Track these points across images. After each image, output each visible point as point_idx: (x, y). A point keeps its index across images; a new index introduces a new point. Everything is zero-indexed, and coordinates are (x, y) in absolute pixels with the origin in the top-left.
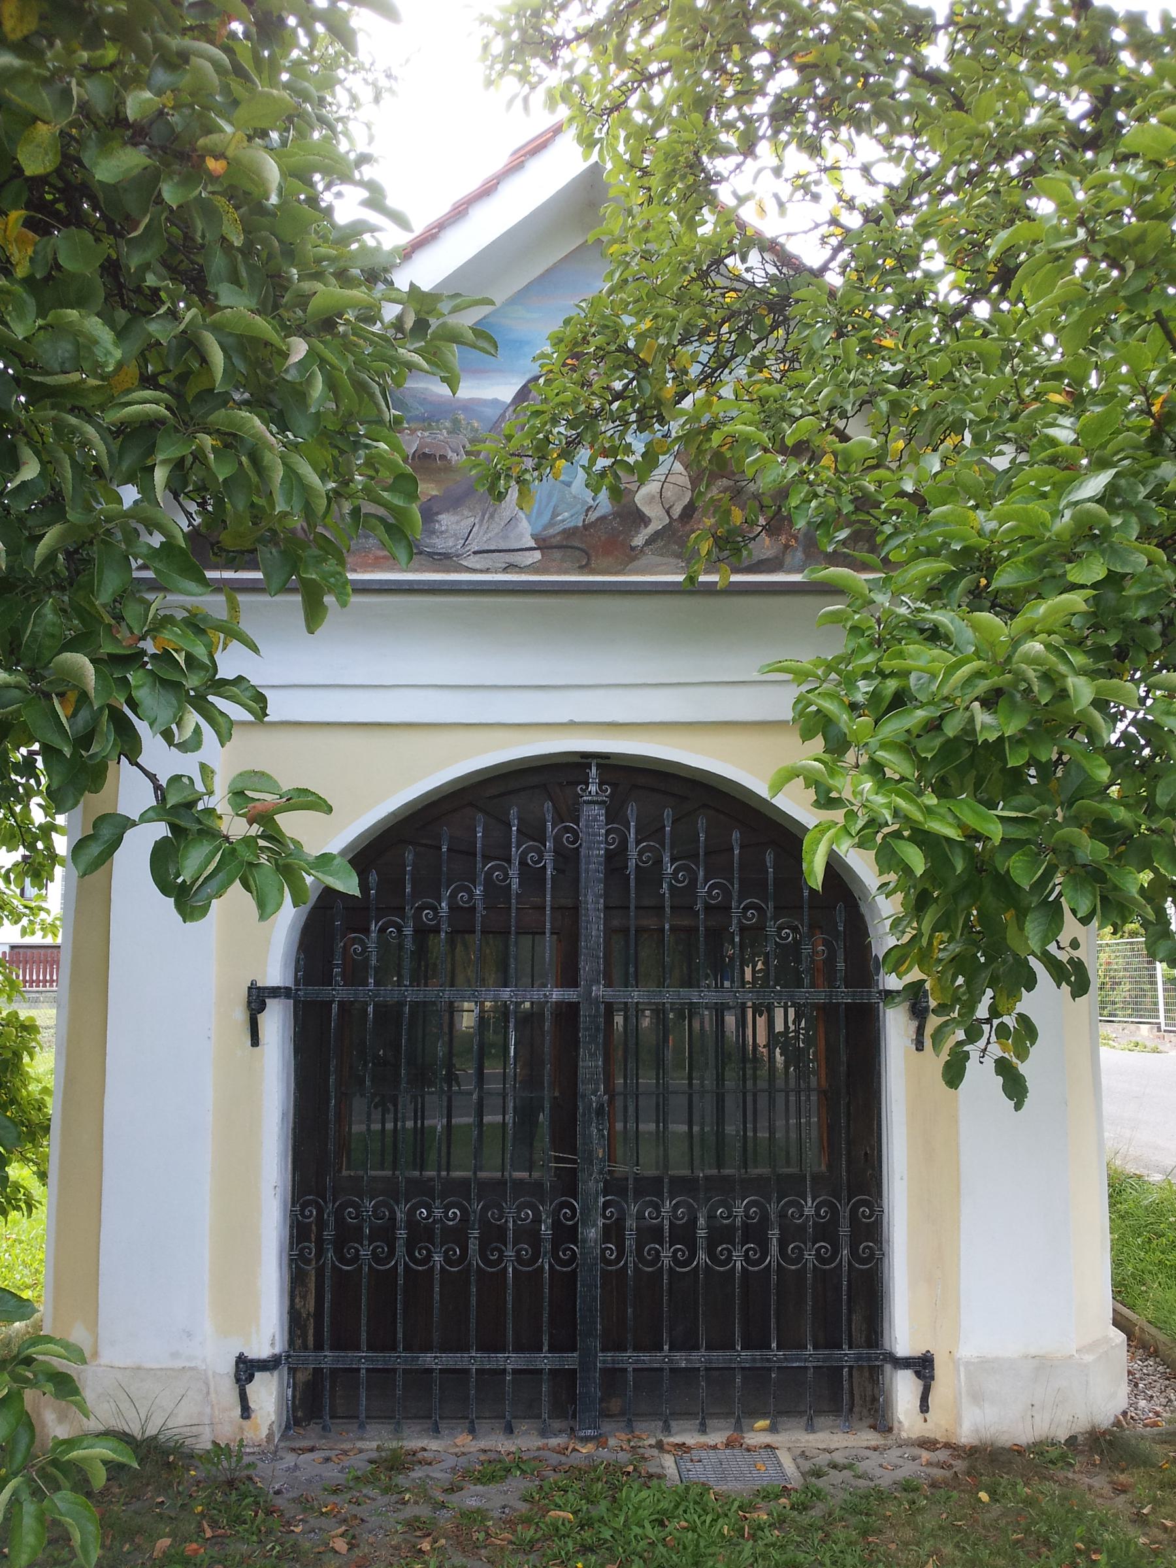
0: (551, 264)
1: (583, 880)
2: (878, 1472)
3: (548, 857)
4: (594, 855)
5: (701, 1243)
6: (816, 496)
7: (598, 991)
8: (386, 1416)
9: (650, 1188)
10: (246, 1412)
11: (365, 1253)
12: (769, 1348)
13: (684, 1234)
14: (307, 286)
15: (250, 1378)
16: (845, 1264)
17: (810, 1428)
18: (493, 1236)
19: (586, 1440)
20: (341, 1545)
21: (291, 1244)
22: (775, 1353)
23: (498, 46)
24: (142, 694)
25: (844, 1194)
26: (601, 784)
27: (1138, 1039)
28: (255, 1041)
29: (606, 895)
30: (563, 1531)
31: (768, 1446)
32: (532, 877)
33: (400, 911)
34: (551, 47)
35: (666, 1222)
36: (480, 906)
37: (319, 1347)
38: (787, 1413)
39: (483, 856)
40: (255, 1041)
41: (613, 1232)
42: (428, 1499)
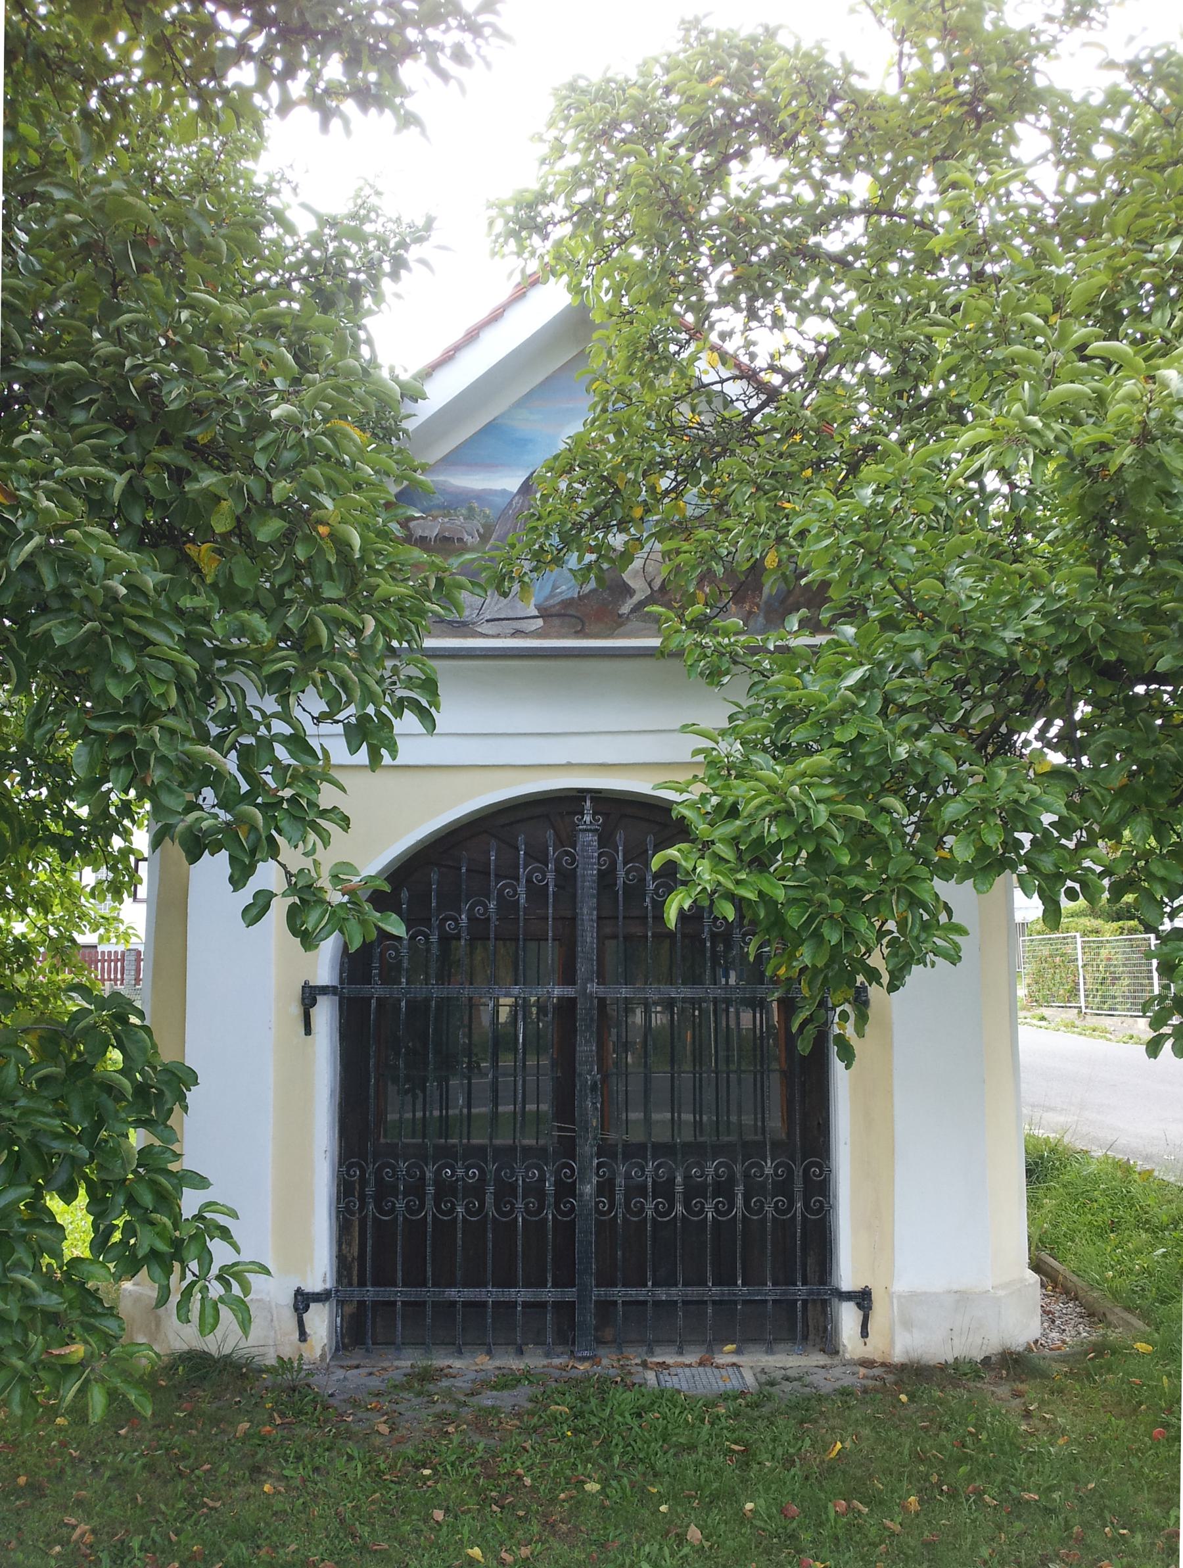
0: (550, 371)
1: (579, 899)
2: (822, 1383)
3: (550, 876)
4: (588, 874)
5: (679, 1197)
6: (706, 656)
7: (593, 988)
8: (419, 1343)
9: (634, 1152)
10: (303, 1336)
11: (400, 1205)
12: (736, 1284)
13: (664, 1189)
14: (374, 580)
15: (307, 1308)
16: (799, 1214)
17: (770, 1351)
18: (506, 1191)
19: (583, 1359)
20: (384, 1429)
21: (338, 1199)
22: (741, 1289)
23: (499, 226)
24: (283, 824)
25: (799, 1156)
26: (594, 814)
27: (1135, 1033)
28: (308, 1030)
29: (599, 908)
30: (560, 1419)
31: (734, 1364)
32: (537, 893)
33: (427, 921)
34: (541, 230)
35: (650, 1180)
36: (494, 917)
37: (362, 1283)
38: (754, 1341)
39: (497, 875)
40: (308, 1030)
41: (605, 1188)
42: (454, 1401)
